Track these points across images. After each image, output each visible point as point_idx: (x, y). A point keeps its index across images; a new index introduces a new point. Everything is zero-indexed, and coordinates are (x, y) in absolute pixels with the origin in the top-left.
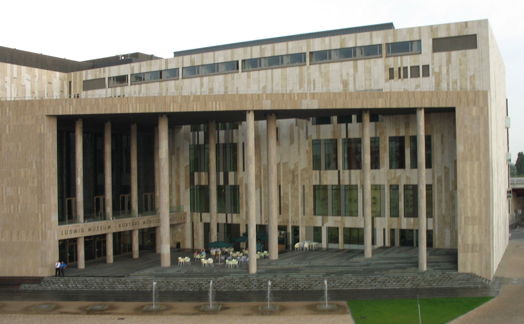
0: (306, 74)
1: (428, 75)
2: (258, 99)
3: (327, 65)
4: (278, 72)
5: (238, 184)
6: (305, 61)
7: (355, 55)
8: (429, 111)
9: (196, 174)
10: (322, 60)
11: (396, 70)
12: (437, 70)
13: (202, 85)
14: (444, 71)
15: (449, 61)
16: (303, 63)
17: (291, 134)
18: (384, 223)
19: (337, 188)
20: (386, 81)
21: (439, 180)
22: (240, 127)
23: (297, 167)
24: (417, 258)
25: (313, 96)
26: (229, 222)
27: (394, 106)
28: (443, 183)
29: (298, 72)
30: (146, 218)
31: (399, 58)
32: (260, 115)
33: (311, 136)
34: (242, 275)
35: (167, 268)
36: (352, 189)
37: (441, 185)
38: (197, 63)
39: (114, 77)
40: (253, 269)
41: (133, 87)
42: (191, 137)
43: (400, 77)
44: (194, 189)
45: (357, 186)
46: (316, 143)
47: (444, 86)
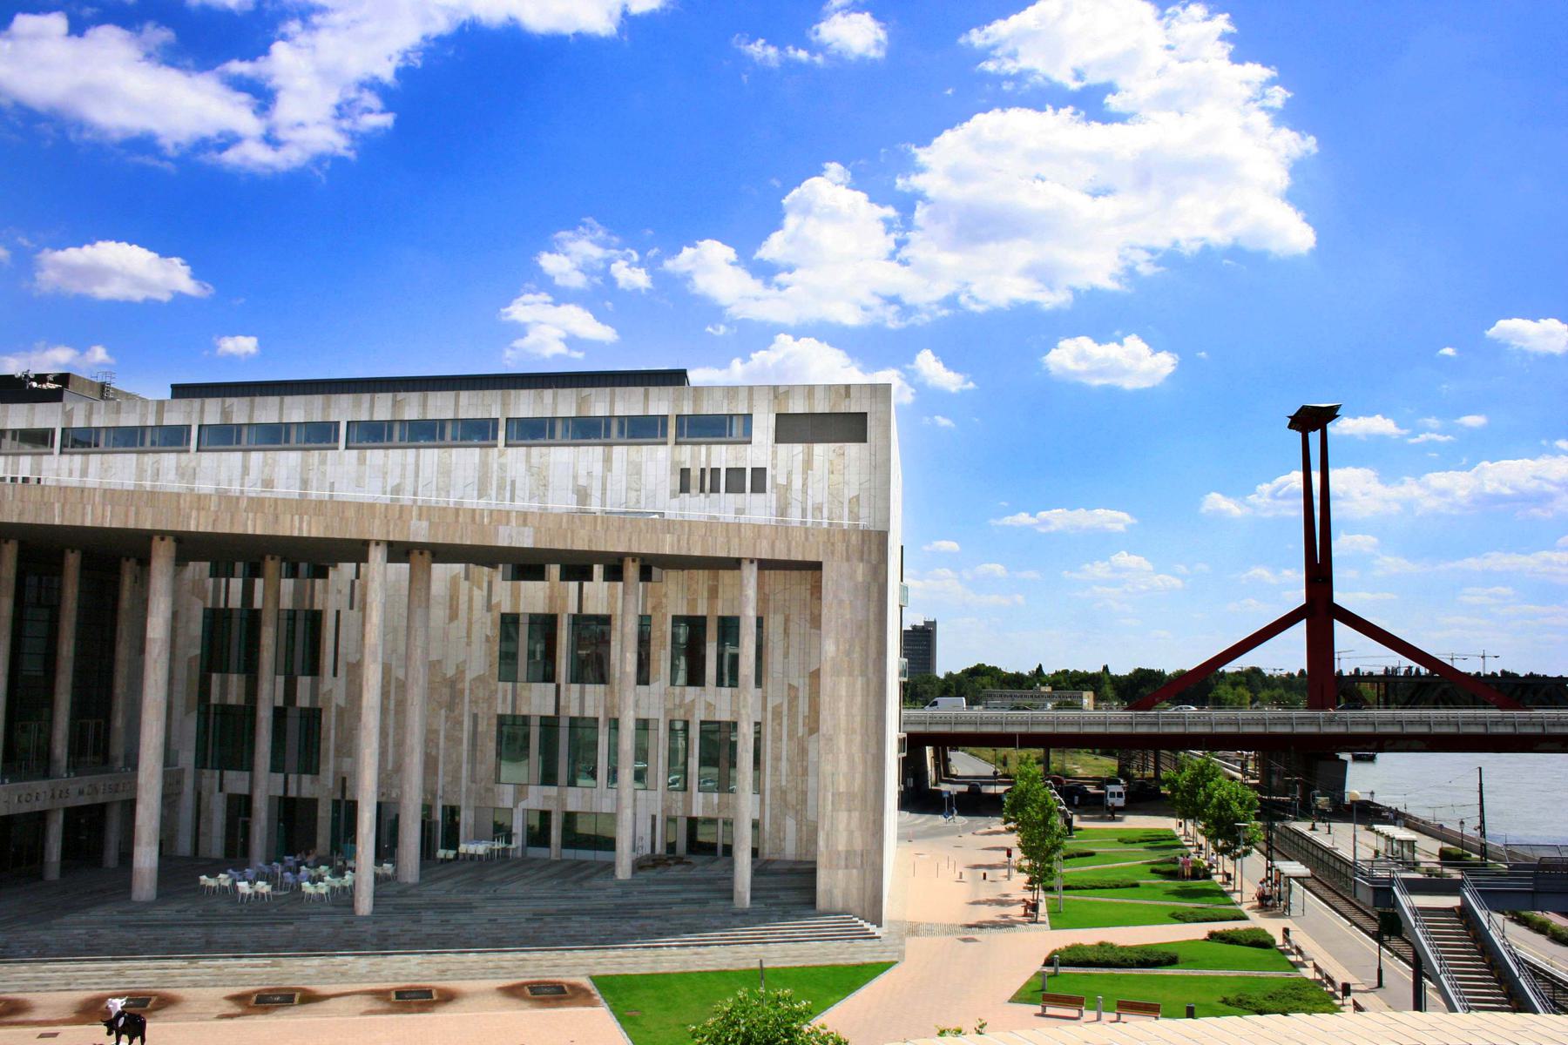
0: (495, 467)
1: (763, 491)
2: (400, 517)
3: (544, 449)
4: (430, 457)
5: (320, 705)
6: (495, 437)
7: (608, 435)
9: (215, 677)
10: (533, 437)
11: (695, 474)
12: (782, 480)
13: (245, 470)
14: (797, 483)
15: (808, 464)
16: (491, 442)
17: (451, 598)
18: (654, 800)
19: (549, 725)
20: (673, 496)
21: (777, 714)
22: (331, 573)
23: (463, 672)
24: (730, 879)
25: (524, 517)
26: (292, 793)
27: (697, 552)
28: (785, 719)
29: (477, 460)
30: (85, 781)
31: (703, 448)
32: (399, 551)
33: (499, 604)
34: (339, 919)
35: (148, 905)
36: (582, 728)
37: (780, 724)
38: (239, 418)
39: (14, 432)
40: (364, 905)
41: (66, 458)
42: (211, 588)
43: (702, 490)
44: (208, 713)
45: (596, 720)
46: (509, 622)
47: (795, 517)
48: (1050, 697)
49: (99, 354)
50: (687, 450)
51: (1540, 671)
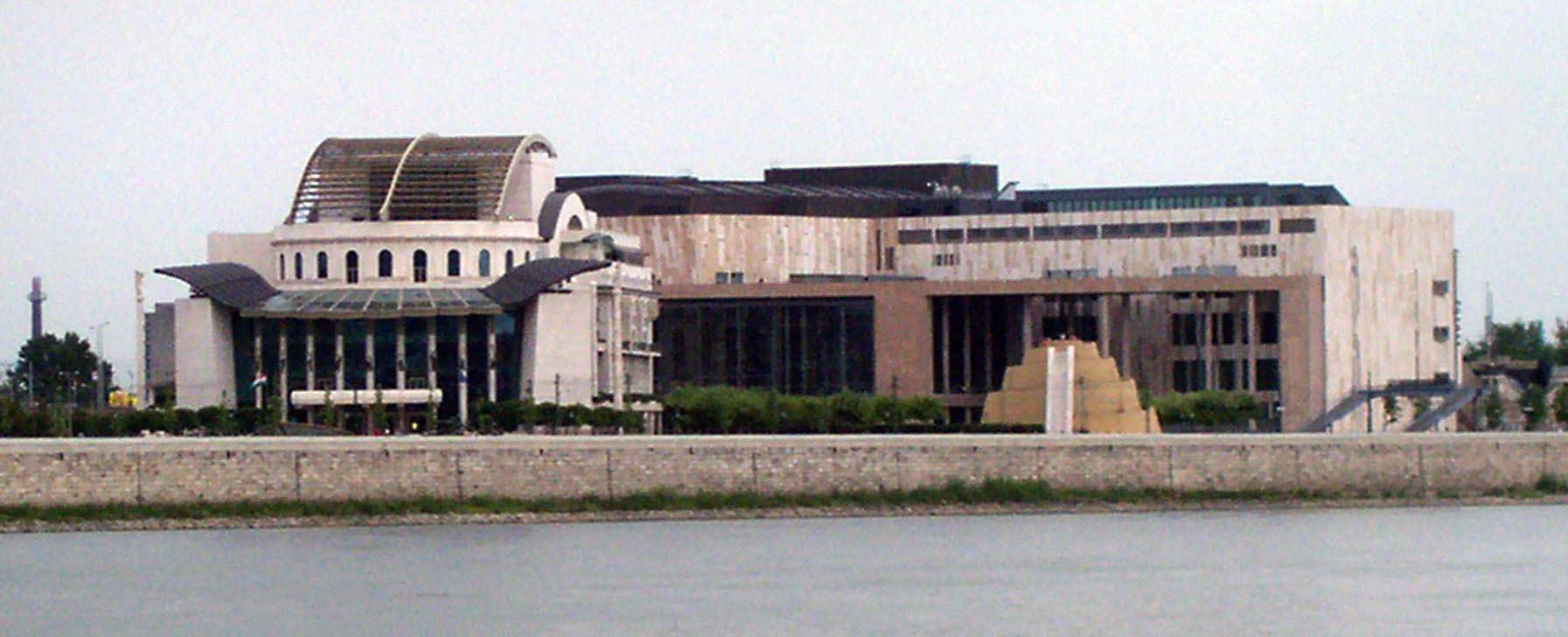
8: (1257, 294)
38: (1052, 223)
46: (1176, 317)
48: (1444, 410)
49: (956, 188)
50: (1244, 237)
51: (446, 132)
